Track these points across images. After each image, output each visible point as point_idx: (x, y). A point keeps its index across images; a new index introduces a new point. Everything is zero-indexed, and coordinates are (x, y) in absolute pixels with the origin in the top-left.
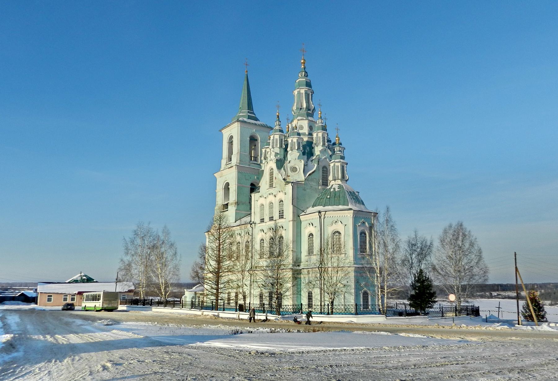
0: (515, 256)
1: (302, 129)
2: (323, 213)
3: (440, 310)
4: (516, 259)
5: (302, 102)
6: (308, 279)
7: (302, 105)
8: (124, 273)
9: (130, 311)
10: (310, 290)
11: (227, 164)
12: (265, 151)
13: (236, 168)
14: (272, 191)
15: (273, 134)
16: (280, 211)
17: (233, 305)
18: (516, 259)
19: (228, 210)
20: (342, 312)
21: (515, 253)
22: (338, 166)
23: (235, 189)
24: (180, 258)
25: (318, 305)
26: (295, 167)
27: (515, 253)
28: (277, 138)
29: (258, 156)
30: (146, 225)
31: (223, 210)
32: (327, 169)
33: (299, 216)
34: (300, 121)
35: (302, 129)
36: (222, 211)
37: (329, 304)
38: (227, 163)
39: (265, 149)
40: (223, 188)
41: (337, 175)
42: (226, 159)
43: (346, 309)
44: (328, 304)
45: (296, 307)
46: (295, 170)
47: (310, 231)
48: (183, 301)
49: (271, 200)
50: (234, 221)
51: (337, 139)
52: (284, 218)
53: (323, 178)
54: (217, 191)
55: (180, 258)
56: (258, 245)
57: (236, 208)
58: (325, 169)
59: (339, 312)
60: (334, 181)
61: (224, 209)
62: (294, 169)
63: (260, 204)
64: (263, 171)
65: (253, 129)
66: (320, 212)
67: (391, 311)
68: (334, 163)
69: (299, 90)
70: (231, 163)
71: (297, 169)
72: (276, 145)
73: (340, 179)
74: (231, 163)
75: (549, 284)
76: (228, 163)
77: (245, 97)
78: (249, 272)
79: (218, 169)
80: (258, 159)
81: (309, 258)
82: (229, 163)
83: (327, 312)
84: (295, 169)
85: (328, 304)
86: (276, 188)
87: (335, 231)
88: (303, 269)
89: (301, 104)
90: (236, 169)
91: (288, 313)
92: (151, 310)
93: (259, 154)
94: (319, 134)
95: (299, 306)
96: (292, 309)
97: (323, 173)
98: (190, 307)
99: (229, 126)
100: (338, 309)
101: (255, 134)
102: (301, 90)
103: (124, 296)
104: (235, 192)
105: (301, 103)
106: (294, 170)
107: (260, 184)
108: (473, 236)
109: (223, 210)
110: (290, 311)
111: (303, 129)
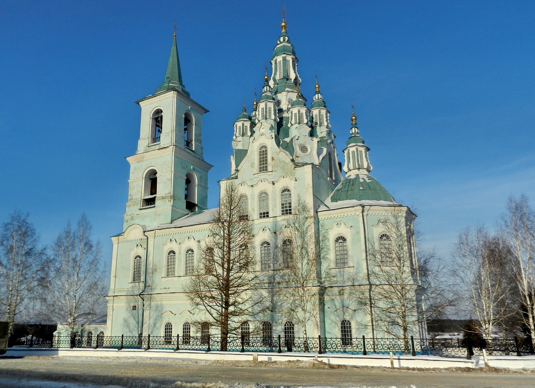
2: (367, 208)
5: (288, 71)
6: (339, 301)
7: (289, 75)
9: (25, 357)
10: (347, 318)
11: (149, 146)
13: (173, 149)
14: (263, 175)
15: (266, 101)
16: (283, 205)
17: (63, 339)
19: (154, 207)
20: (400, 350)
22: (354, 152)
23: (171, 179)
24: (104, 268)
25: (136, 337)
26: (305, 146)
28: (270, 106)
29: (192, 141)
30: (23, 217)
31: (143, 206)
33: (317, 212)
34: (290, 93)
36: (141, 208)
38: (149, 144)
39: (243, 122)
40: (144, 176)
41: (361, 163)
42: (148, 139)
43: (358, 346)
45: (157, 340)
47: (339, 234)
48: (412, 338)
49: (285, 185)
50: (169, 221)
51: (354, 118)
52: (269, 217)
54: (129, 181)
55: (104, 268)
57: (172, 204)
59: (394, 350)
60: (357, 170)
61: (144, 205)
63: (259, 191)
65: (189, 106)
66: (363, 207)
67: (217, 342)
68: (357, 147)
69: (285, 55)
70: (159, 144)
72: (270, 116)
73: (365, 169)
74: (159, 144)
76: (151, 144)
77: (175, 65)
78: (141, 296)
79: (133, 151)
80: (192, 145)
81: (340, 272)
82: (152, 144)
83: (363, 350)
86: (273, 172)
87: (383, 233)
88: (331, 287)
89: (288, 73)
90: (173, 151)
92: (57, 354)
93: (192, 139)
94: (321, 111)
95: (162, 338)
98: (68, 345)
99: (160, 95)
101: (190, 113)
102: (288, 56)
104: (169, 182)
105: (288, 72)
106: (303, 150)
107: (239, 167)
109: (143, 206)
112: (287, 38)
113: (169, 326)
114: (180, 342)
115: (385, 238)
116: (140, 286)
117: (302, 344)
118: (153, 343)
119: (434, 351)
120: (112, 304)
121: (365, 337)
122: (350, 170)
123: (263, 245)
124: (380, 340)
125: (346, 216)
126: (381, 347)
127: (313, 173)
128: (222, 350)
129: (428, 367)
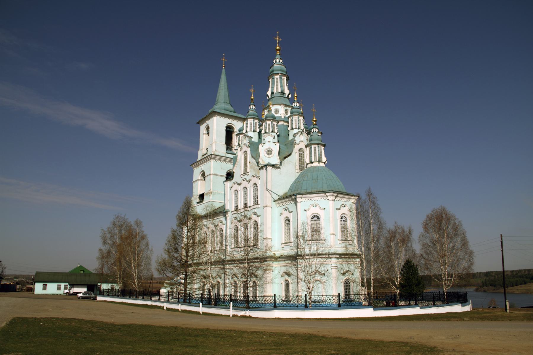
0: (502, 239)
1: (277, 113)
3: (246, 295)
4: (502, 242)
8: (125, 274)
12: (207, 269)
18: (502, 242)
21: (501, 235)
27: (501, 235)
32: (304, 153)
35: (277, 113)
37: (307, 295)
44: (306, 295)
46: (270, 152)
53: (300, 161)
56: (229, 228)
58: (301, 153)
62: (268, 152)
64: (237, 156)
71: (270, 155)
75: (492, 272)
83: (338, 303)
84: (270, 153)
85: (306, 295)
87: (318, 216)
91: (268, 304)
96: (281, 301)
97: (300, 156)
100: (332, 300)
103: (44, 286)
108: (406, 232)
110: (264, 303)
111: (278, 113)
112: (281, 61)
113: (346, 284)
114: (277, 301)
115: (315, 218)
116: (308, 249)
117: (296, 300)
118: (295, 301)
119: (348, 302)
120: (149, 285)
121: (340, 294)
122: (312, 162)
123: (313, 219)
124: (428, 293)
125: (312, 200)
126: (329, 301)
127: (40, 272)
128: (208, 305)
129: (220, 314)
